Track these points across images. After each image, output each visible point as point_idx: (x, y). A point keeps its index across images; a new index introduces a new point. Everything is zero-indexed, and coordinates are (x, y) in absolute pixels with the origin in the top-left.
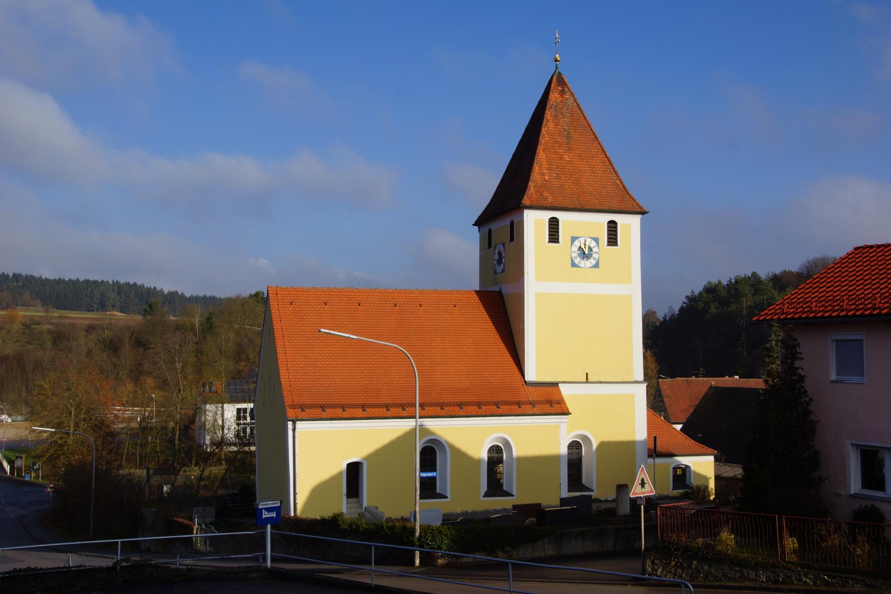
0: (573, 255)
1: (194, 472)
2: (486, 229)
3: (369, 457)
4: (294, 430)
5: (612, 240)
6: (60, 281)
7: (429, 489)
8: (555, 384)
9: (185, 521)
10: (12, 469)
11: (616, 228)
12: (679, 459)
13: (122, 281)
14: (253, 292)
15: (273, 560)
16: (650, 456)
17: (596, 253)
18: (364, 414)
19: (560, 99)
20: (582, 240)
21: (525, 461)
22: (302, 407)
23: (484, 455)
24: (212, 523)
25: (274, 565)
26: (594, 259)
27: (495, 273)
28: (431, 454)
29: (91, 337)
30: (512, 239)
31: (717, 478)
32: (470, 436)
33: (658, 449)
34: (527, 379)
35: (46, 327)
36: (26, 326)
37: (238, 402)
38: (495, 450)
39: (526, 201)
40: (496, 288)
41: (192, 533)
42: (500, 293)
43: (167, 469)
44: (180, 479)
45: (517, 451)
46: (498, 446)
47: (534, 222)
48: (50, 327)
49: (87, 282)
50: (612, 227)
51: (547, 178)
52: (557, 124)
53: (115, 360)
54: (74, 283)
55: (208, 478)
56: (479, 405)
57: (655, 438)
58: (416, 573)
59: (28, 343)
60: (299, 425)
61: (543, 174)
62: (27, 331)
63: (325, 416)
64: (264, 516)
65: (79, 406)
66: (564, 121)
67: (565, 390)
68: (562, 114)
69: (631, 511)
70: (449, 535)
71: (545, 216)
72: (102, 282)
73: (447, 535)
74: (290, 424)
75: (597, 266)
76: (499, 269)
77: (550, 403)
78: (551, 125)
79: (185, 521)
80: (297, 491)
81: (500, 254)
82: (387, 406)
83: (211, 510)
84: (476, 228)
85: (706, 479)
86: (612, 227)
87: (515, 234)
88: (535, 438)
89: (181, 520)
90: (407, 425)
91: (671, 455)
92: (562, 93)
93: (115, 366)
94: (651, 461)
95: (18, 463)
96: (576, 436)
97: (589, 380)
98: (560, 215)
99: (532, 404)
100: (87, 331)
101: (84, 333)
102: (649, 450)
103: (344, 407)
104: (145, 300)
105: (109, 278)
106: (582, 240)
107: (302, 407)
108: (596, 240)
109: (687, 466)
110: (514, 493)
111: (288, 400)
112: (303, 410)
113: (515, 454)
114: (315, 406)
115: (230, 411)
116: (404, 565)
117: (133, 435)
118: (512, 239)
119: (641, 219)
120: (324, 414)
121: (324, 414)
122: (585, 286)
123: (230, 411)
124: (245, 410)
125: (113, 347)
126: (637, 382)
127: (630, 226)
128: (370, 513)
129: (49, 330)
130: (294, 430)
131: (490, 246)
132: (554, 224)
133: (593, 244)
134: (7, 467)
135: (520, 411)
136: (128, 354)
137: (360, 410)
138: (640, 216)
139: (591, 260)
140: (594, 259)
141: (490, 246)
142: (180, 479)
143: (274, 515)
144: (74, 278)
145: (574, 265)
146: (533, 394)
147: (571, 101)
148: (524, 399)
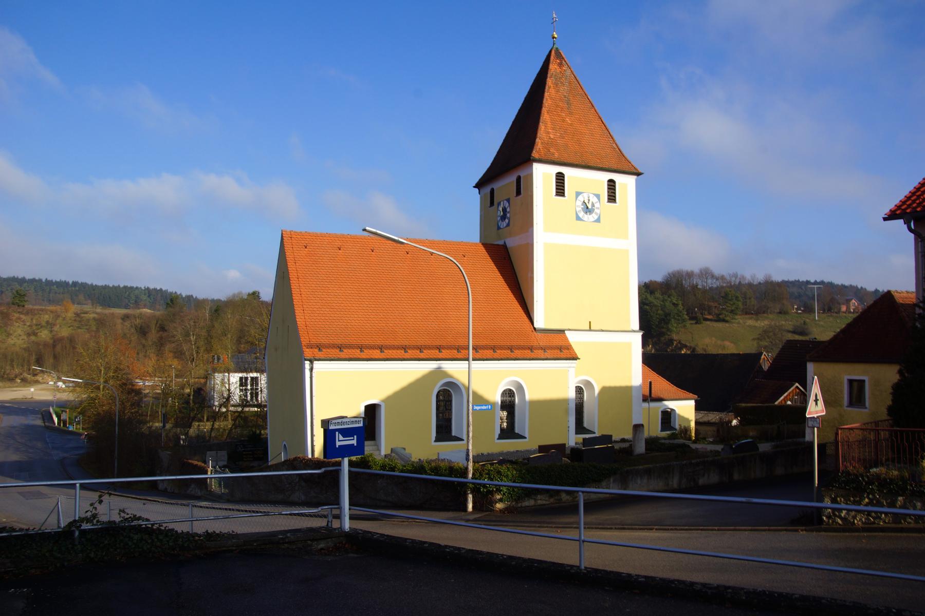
0: (578, 209)
1: (206, 426)
2: (487, 190)
3: (388, 400)
4: (311, 370)
5: (612, 198)
6: (105, 287)
7: (444, 431)
9: (199, 463)
10: (59, 423)
11: (615, 186)
12: (666, 403)
13: (152, 287)
14: (251, 291)
15: (352, 518)
18: (383, 355)
19: (558, 70)
20: (585, 195)
21: (536, 404)
22: (320, 347)
24: (225, 466)
25: (354, 526)
26: (596, 214)
27: (499, 228)
28: (447, 397)
29: (126, 324)
30: (518, 193)
31: (697, 423)
32: (487, 379)
34: (537, 325)
35: (92, 316)
36: (77, 315)
37: (242, 372)
38: (508, 393)
39: (535, 154)
40: (501, 243)
41: (206, 473)
42: (505, 246)
43: (185, 421)
44: (192, 431)
46: (510, 390)
47: (542, 175)
48: (95, 315)
49: (125, 287)
50: (612, 184)
51: (552, 136)
52: (558, 91)
53: (144, 341)
54: (116, 288)
55: (218, 430)
56: (494, 348)
57: (650, 383)
58: (468, 520)
59: (79, 328)
60: (317, 364)
61: (548, 133)
62: (78, 319)
63: (343, 356)
64: (338, 444)
65: (107, 368)
66: (564, 89)
67: (572, 337)
68: (562, 83)
69: (646, 449)
70: (510, 476)
72: (137, 288)
73: (507, 476)
74: (307, 363)
75: (598, 220)
76: (505, 224)
77: (560, 348)
78: (552, 91)
79: (199, 463)
80: (315, 433)
81: (504, 210)
82: (405, 348)
83: (224, 454)
84: (477, 190)
85: (688, 421)
86: (612, 184)
87: (523, 189)
88: (544, 382)
89: (195, 463)
90: (430, 366)
91: (661, 400)
92: (560, 65)
93: (144, 346)
94: (646, 405)
95: (64, 416)
96: (579, 382)
98: (567, 171)
99: (544, 349)
100: (123, 319)
101: (120, 321)
103: (361, 348)
104: (171, 301)
105: (142, 285)
107: (320, 347)
108: (598, 196)
109: (672, 410)
110: (526, 435)
111: (304, 340)
112: (320, 350)
113: (529, 396)
114: (333, 346)
115: (235, 378)
116: (453, 510)
117: (157, 398)
118: (518, 193)
119: (636, 180)
120: (342, 355)
121: (342, 355)
122: (587, 238)
123: (235, 378)
124: (246, 378)
125: (143, 331)
126: (634, 331)
127: (626, 184)
128: (397, 454)
129: (94, 319)
130: (311, 370)
131: (492, 203)
132: (560, 178)
133: (594, 200)
134: (56, 420)
135: (533, 355)
136: (153, 335)
137: (378, 351)
138: (635, 177)
140: (596, 214)
141: (492, 203)
142: (192, 431)
143: (354, 442)
144: (116, 285)
145: (578, 218)
146: (542, 340)
147: (568, 72)
148: (535, 344)
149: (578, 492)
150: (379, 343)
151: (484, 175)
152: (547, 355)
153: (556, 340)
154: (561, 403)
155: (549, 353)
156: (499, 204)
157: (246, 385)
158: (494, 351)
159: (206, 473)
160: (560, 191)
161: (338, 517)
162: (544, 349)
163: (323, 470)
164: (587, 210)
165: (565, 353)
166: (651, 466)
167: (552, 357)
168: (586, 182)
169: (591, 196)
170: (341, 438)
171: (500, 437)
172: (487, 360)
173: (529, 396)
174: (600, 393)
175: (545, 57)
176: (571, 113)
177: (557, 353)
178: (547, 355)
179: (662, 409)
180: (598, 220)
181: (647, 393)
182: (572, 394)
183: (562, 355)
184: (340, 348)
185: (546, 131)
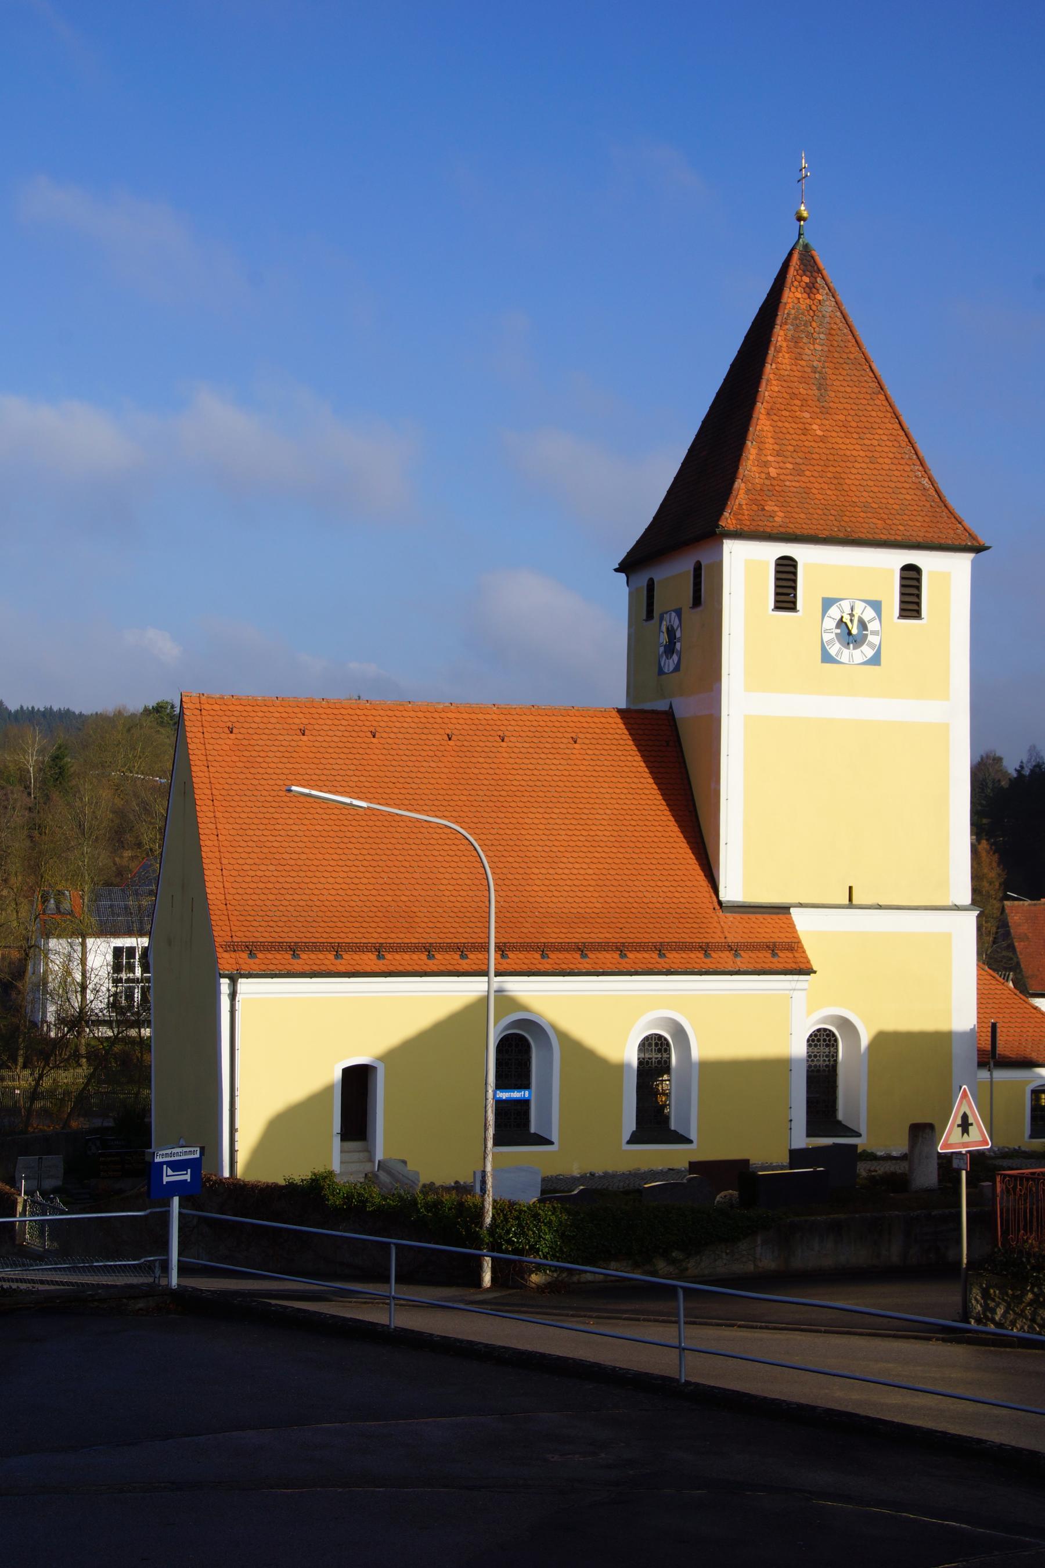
0: (827, 637)
2: (642, 580)
3: (392, 1056)
4: (233, 996)
5: (911, 604)
14: (151, 704)
16: (982, 1064)
17: (875, 633)
18: (381, 965)
19: (805, 303)
21: (713, 1069)
22: (251, 949)
26: (871, 645)
27: (661, 672)
28: (519, 1050)
30: (697, 601)
32: (603, 1015)
33: (1001, 1049)
37: (116, 934)
39: (728, 521)
40: (661, 706)
42: (669, 716)
46: (660, 1037)
47: (744, 567)
50: (911, 576)
51: (773, 472)
52: (799, 357)
55: (51, 1093)
56: (621, 949)
60: (245, 986)
61: (766, 464)
64: (166, 1179)
66: (814, 351)
70: (555, 1224)
75: (875, 660)
77: (773, 949)
81: (671, 632)
82: (429, 950)
83: (55, 1162)
84: (622, 577)
86: (911, 576)
87: (705, 592)
88: (738, 1023)
90: (467, 990)
92: (811, 289)
94: (984, 1074)
96: (825, 1020)
97: (855, 901)
99: (734, 949)
106: (846, 606)
107: (251, 949)
108: (876, 606)
110: (693, 1136)
111: (221, 934)
113: (697, 1053)
115: (100, 953)
118: (697, 601)
120: (297, 965)
121: (297, 965)
123: (100, 953)
126: (957, 908)
127: (949, 575)
128: (389, 1173)
130: (233, 996)
131: (650, 615)
132: (786, 569)
133: (869, 614)
135: (708, 963)
137: (373, 956)
138: (971, 556)
140: (871, 645)
141: (650, 615)
145: (827, 658)
146: (734, 929)
147: (829, 307)
148: (717, 938)
149: (390, 1243)
150: (374, 939)
151: (639, 543)
152: (740, 963)
153: (766, 929)
154: (775, 1068)
155: (745, 960)
156: (661, 619)
157: (131, 968)
158: (623, 956)
159: (15, 1216)
160: (786, 598)
161: (165, 1267)
162: (734, 949)
163: (148, 1211)
164: (851, 635)
165: (785, 958)
166: (842, 1216)
167: (751, 968)
168: (849, 574)
169: (859, 607)
170: (170, 1172)
171: (628, 1142)
172: (604, 974)
173: (697, 1053)
175: (788, 252)
176: (825, 411)
177: (764, 958)
178: (740, 963)
179: (1033, 1085)
182: (799, 1049)
183: (776, 963)
184: (294, 949)
185: (760, 460)
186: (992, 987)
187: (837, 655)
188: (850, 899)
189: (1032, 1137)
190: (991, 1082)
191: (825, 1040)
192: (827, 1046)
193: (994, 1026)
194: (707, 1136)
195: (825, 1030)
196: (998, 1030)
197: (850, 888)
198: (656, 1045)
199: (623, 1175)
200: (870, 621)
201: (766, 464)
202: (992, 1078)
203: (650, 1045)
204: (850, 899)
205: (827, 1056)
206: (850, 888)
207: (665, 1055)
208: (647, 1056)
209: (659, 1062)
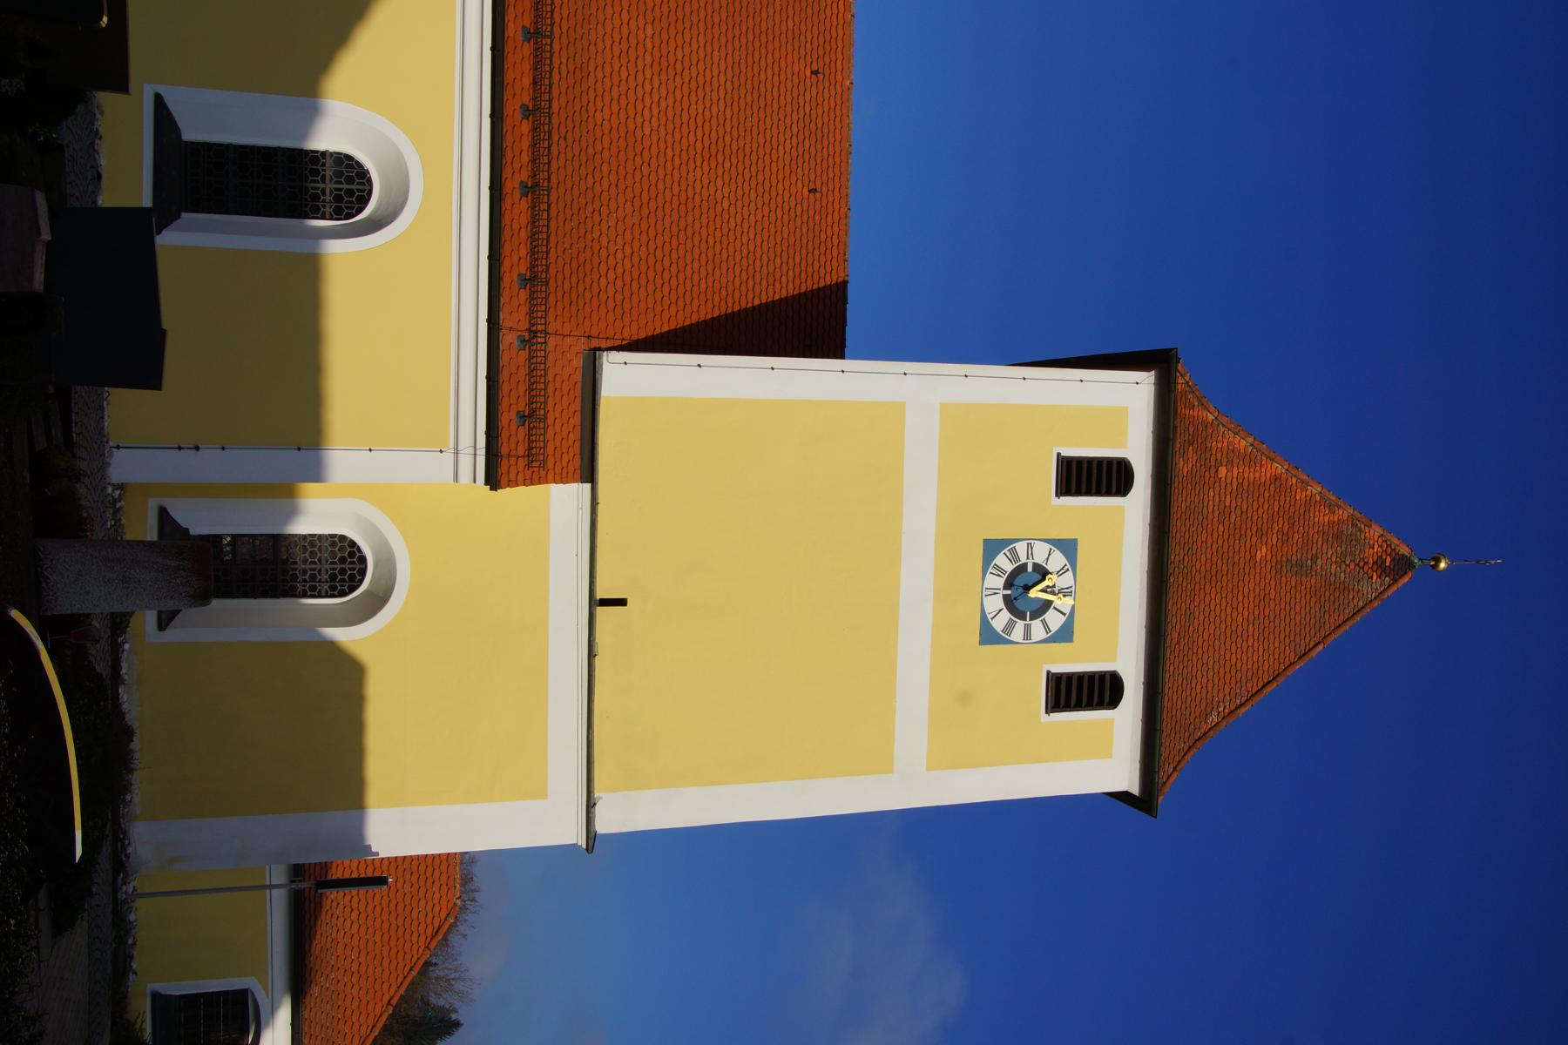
8: (589, 474)
12: (284, 1016)
16: (297, 871)
17: (1027, 630)
21: (306, 280)
23: (327, 138)
26: (1009, 627)
33: (332, 895)
45: (345, 257)
46: (362, 175)
50: (1097, 691)
67: (563, 500)
71: (1136, 446)
75: (989, 636)
86: (1097, 691)
91: (299, 990)
94: (278, 875)
97: (600, 610)
102: (325, 867)
106: (1066, 581)
108: (1065, 634)
113: (336, 249)
122: (928, 590)
133: (1054, 620)
139: (1006, 615)
140: (1009, 627)
164: (1022, 591)
165: (514, 438)
171: (163, 512)
173: (336, 249)
174: (333, 648)
180: (989, 636)
181: (336, 874)
186: (422, 929)
187: (996, 567)
188: (606, 602)
189: (156, 996)
190: (265, 887)
191: (343, 571)
192: (333, 577)
193: (382, 881)
194: (172, 657)
195: (363, 573)
196: (377, 889)
197: (622, 602)
198: (350, 193)
199: (91, 151)
200: (1044, 623)
201: (1230, 463)
202: (271, 887)
203: (350, 180)
204: (606, 602)
205: (313, 577)
206: (622, 602)
207: (328, 210)
208: (329, 173)
209: (316, 197)
